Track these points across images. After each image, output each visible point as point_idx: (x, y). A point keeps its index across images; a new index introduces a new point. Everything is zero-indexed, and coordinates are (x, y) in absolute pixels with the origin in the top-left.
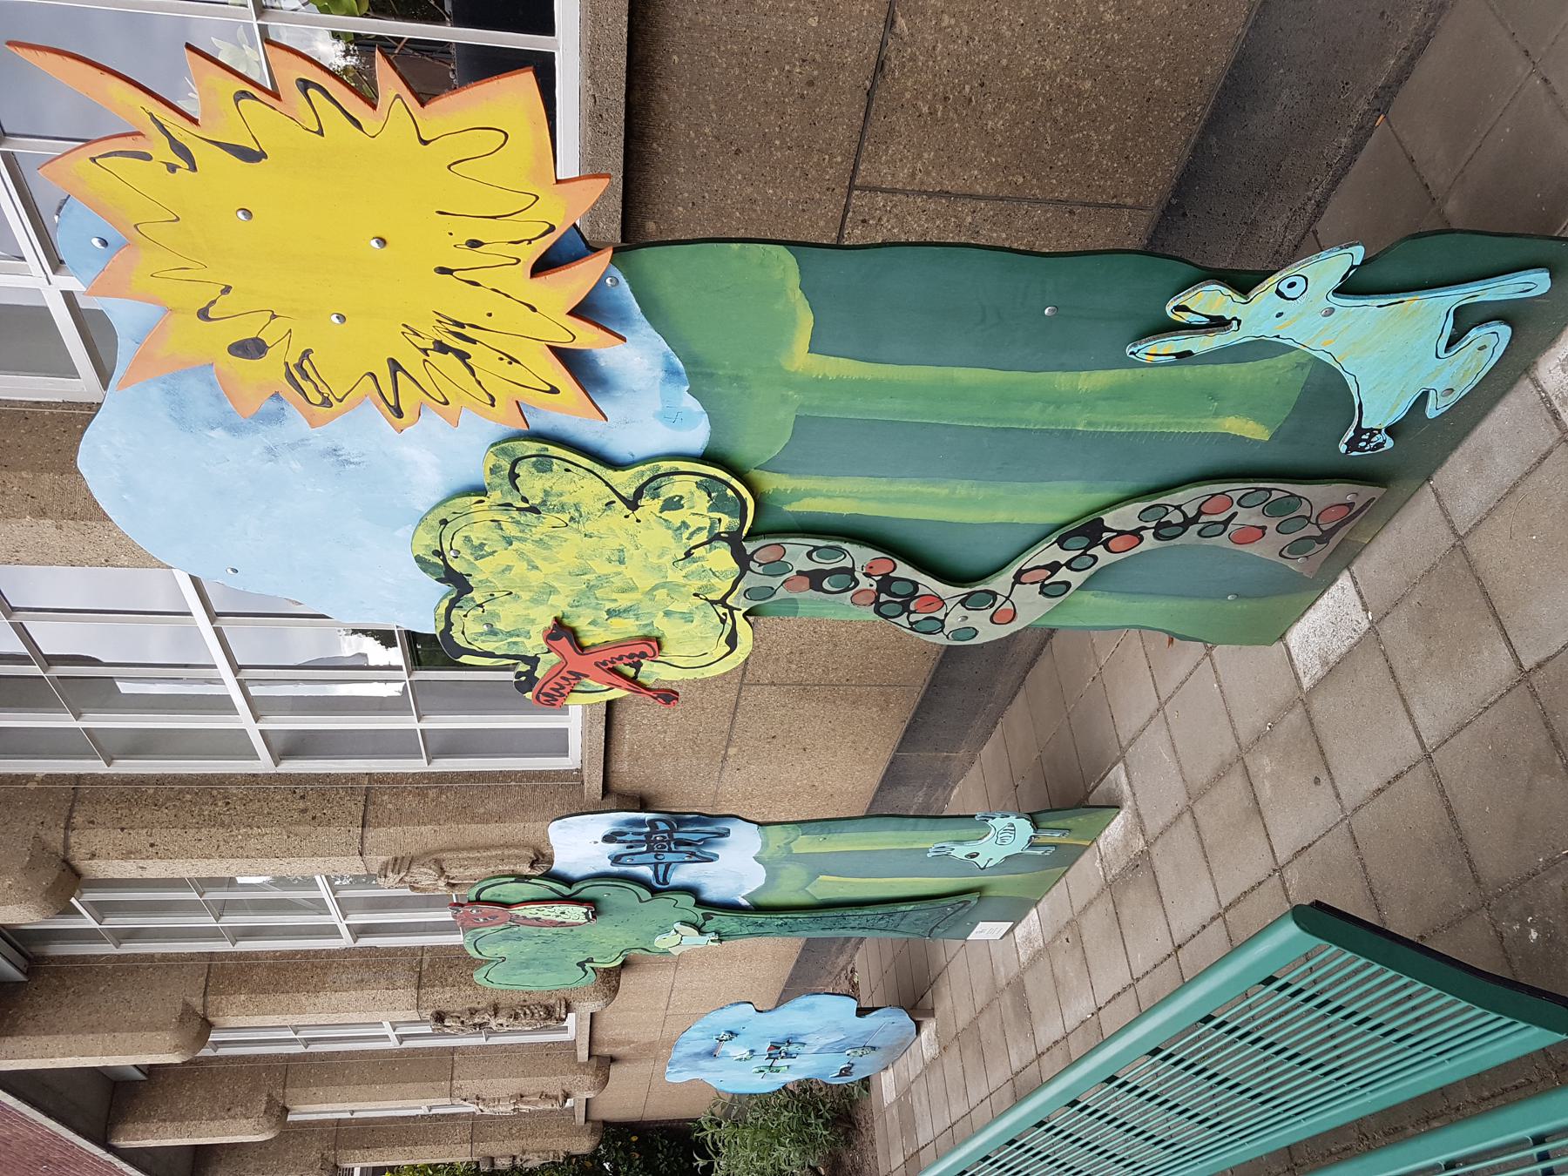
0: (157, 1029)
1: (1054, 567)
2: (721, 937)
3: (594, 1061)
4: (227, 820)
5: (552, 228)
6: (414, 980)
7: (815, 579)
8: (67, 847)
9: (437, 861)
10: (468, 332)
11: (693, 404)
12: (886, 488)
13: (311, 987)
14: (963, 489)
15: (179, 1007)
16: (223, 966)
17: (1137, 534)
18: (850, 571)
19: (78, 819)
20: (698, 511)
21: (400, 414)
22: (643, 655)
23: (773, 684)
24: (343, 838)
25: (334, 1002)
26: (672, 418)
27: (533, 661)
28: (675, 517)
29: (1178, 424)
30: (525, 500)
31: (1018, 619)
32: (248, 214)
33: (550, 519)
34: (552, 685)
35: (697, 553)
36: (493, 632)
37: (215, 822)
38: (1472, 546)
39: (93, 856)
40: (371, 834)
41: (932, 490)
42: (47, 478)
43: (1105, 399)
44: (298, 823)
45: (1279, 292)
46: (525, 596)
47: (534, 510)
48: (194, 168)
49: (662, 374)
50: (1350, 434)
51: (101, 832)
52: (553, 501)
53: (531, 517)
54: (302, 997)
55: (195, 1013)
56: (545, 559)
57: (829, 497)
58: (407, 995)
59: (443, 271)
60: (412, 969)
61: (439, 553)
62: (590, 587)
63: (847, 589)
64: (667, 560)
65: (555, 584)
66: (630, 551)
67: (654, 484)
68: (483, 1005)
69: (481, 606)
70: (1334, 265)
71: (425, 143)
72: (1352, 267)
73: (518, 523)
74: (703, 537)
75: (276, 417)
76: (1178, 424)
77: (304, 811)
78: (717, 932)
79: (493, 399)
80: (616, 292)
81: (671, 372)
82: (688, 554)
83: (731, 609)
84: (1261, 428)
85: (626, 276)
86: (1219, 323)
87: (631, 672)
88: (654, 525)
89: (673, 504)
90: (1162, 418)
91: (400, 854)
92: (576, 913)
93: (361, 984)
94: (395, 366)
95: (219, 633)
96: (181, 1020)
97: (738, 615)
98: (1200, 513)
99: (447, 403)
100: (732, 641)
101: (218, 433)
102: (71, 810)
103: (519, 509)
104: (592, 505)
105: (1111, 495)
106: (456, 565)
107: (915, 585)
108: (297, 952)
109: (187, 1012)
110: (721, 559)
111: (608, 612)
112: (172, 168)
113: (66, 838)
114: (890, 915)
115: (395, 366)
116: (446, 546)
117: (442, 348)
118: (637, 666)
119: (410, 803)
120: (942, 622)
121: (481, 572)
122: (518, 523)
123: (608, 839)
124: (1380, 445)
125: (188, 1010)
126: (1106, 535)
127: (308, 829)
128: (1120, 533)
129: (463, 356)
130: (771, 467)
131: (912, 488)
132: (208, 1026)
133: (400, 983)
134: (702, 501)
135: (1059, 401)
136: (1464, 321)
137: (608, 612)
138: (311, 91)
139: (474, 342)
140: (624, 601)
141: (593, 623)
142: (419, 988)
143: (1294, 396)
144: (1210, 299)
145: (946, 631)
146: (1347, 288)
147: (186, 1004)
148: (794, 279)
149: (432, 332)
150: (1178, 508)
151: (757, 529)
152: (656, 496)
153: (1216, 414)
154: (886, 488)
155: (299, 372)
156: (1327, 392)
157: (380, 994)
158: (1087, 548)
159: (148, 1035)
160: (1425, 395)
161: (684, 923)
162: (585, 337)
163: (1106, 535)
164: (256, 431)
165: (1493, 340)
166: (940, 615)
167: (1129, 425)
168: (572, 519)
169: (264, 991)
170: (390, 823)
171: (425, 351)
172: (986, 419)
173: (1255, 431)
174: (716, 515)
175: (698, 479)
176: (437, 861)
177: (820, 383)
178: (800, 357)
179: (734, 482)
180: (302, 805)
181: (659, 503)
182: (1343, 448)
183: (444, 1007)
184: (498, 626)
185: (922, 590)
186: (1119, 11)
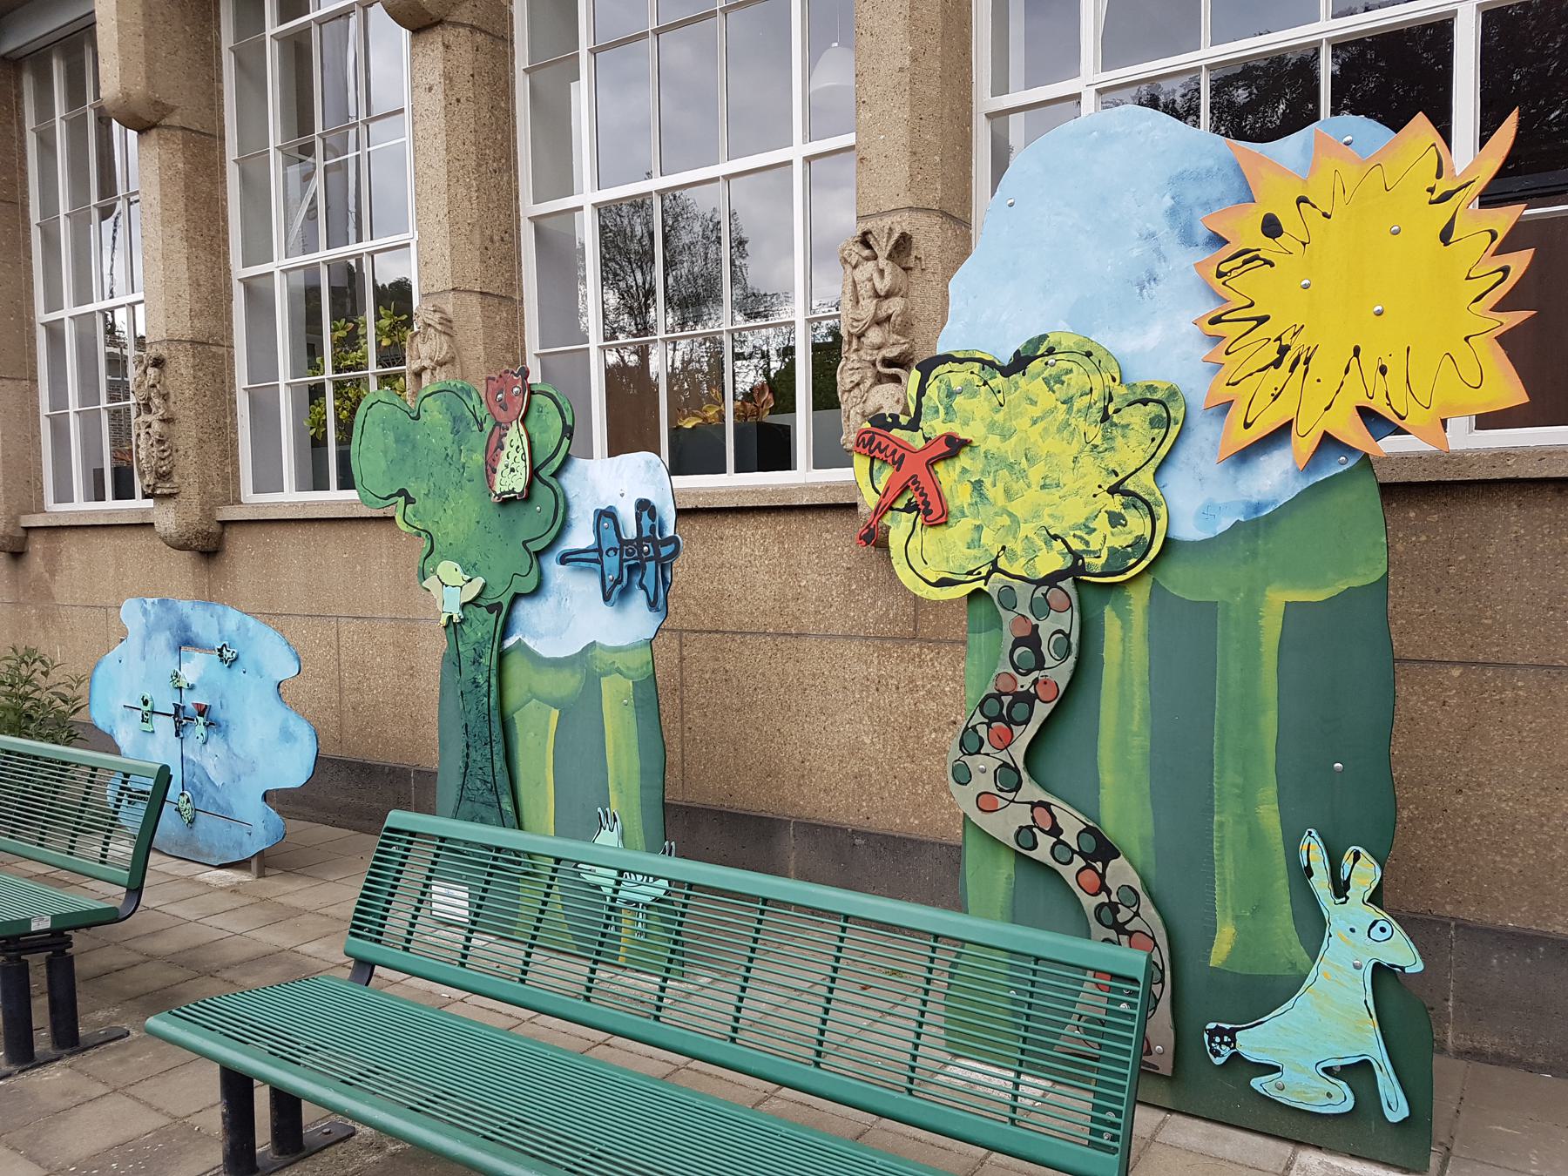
1: (1055, 831)
2: (453, 627)
3: (21, 534)
4: (483, 169)
7: (1031, 640)
8: (455, 24)
10: (1301, 367)
11: (1225, 524)
12: (1137, 681)
14: (1140, 742)
15: (170, 102)
16: (214, 149)
18: (1040, 665)
19: (479, 38)
20: (1104, 541)
21: (1213, 322)
22: (927, 512)
23: (682, 659)
25: (176, 256)
27: (914, 425)
28: (1102, 523)
30: (1117, 411)
32: (1396, 233)
35: (1058, 545)
36: (951, 394)
37: (481, 159)
38: (1155, 1148)
39: (447, 47)
40: (475, 300)
41: (1137, 717)
42: (937, 65)
45: (1375, 922)
46: (999, 417)
47: (1105, 417)
48: (1431, 202)
49: (1254, 500)
50: (1228, 1027)
51: (470, 57)
52: (1117, 432)
53: (1099, 417)
55: (163, 117)
57: (1123, 640)
58: (183, 329)
59: (1357, 351)
60: (211, 336)
61: (1051, 351)
62: (1011, 466)
64: (1047, 521)
65: (1014, 439)
66: (1056, 494)
67: (1139, 503)
68: (173, 408)
69: (985, 383)
70: (1402, 953)
71: (1466, 339)
72: (1402, 969)
73: (1090, 407)
74: (1076, 545)
75: (1187, 238)
77: (492, 240)
78: (463, 621)
81: (1258, 507)
82: (1055, 537)
83: (987, 578)
86: (1340, 888)
87: (901, 504)
89: (1115, 520)
90: (1230, 877)
91: (455, 325)
93: (196, 284)
94: (1262, 320)
95: (716, 179)
97: (980, 584)
99: (1227, 353)
100: (943, 583)
101: (1168, 202)
104: (1112, 461)
105: (1138, 859)
106: (1036, 366)
107: (1027, 722)
108: (225, 220)
110: (1052, 561)
111: (980, 482)
112: (1431, 190)
113: (463, 25)
115: (1262, 320)
117: (1283, 350)
119: (502, 337)
120: (978, 752)
121: (1030, 383)
122: (1090, 407)
123: (644, 506)
124: (1217, 1054)
125: (169, 110)
126: (1099, 865)
127: (478, 242)
128: (1102, 876)
129: (1277, 364)
130: (1156, 588)
131: (1137, 702)
132: (143, 129)
133: (197, 323)
134: (1121, 540)
136: (1358, 1073)
137: (980, 482)
138: (1500, 274)
139: (1292, 370)
142: (192, 342)
143: (1261, 971)
146: (1381, 973)
147: (172, 109)
149: (1297, 346)
150: (1137, 914)
151: (1084, 585)
152: (1125, 506)
153: (1236, 918)
154: (1137, 681)
156: (1267, 992)
157: (185, 304)
158: (1081, 854)
159: (142, 68)
161: (485, 586)
162: (1303, 444)
163: (1099, 865)
164: (1172, 228)
165: (1341, 1099)
166: (986, 748)
168: (1096, 446)
169: (187, 187)
170: (486, 317)
173: (1220, 952)
175: (1148, 536)
178: (1277, 599)
179: (1144, 563)
180: (496, 238)
181: (1118, 509)
182: (1211, 1026)
183: (171, 366)
184: (959, 399)
185: (1017, 730)
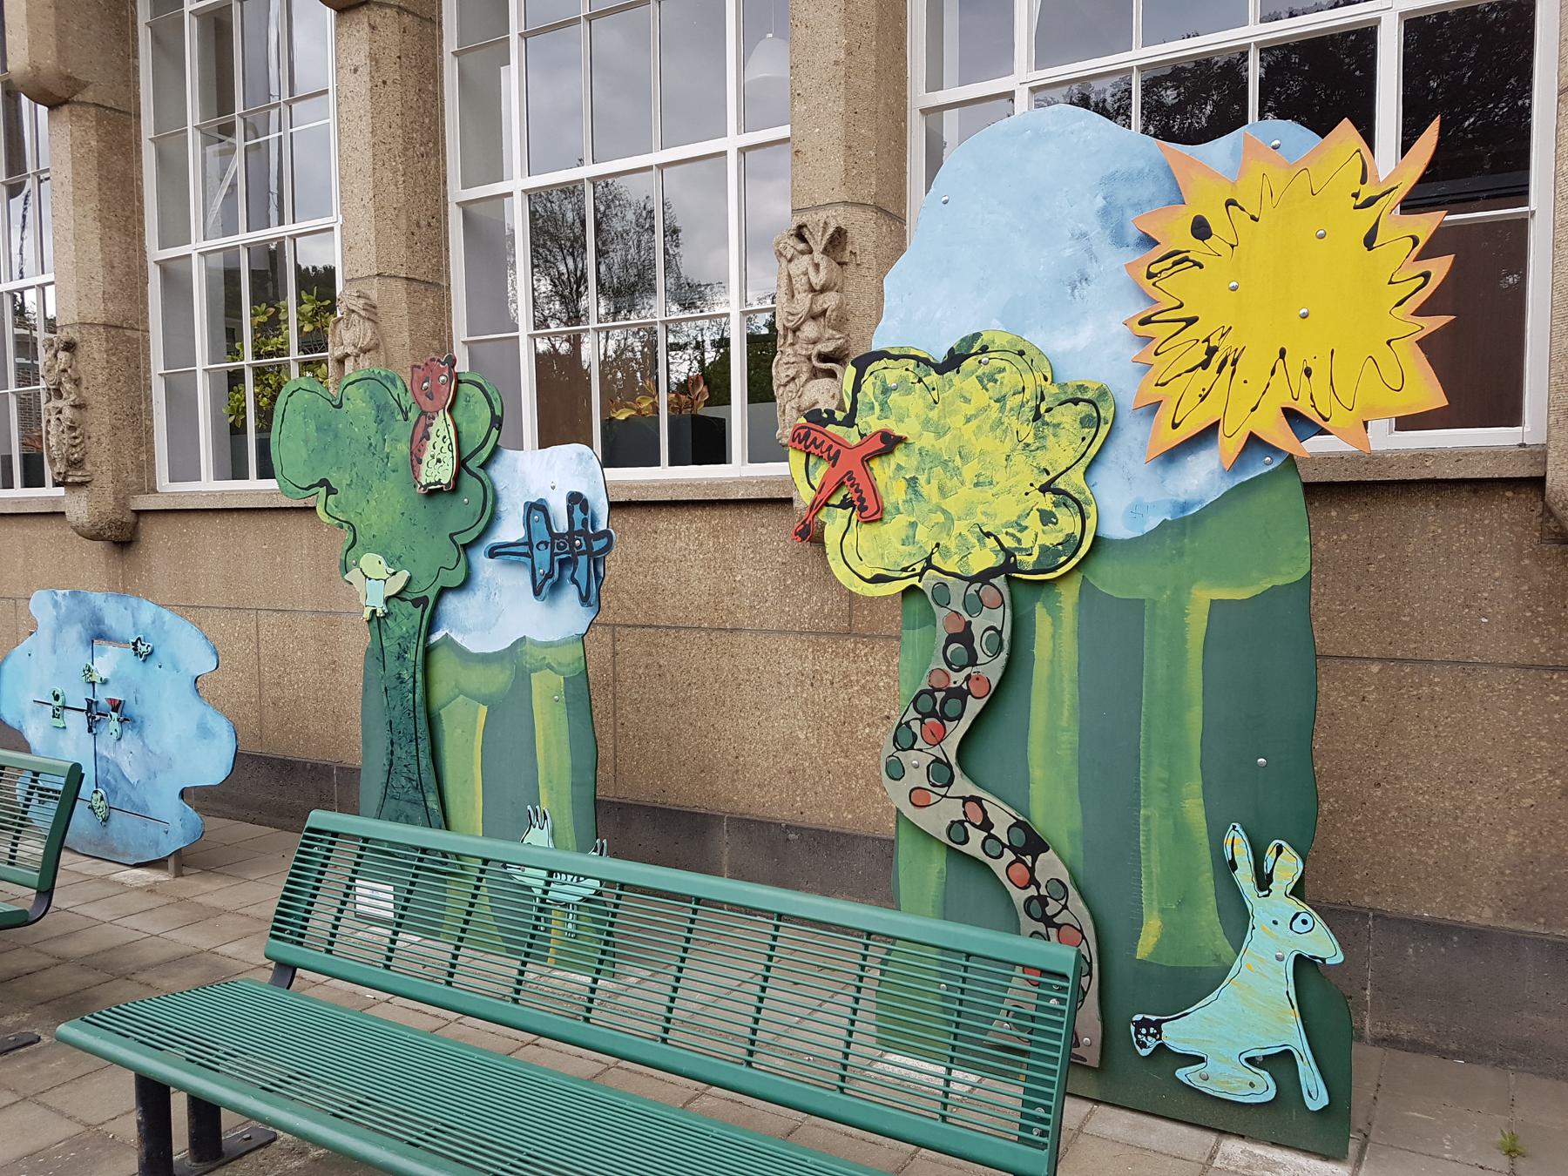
0: (59, 52)
1: (986, 825)
4: (410, 153)
5: (1326, 420)
6: (113, 321)
9: (377, 345)
10: (1228, 368)
11: (1153, 523)
13: (105, 214)
14: (1069, 738)
15: (82, 78)
16: (129, 127)
17: (1033, 881)
18: (973, 661)
19: (407, 19)
20: (1035, 539)
21: (1143, 322)
23: (615, 654)
24: (395, 259)
25: (89, 236)
26: (1136, 511)
27: (849, 421)
29: (1151, 884)
30: (1048, 410)
31: (918, 810)
32: (1321, 237)
33: (1027, 431)
34: (820, 438)
35: (991, 542)
37: (408, 143)
41: (1066, 714)
43: (1175, 824)
44: (408, 218)
46: (934, 414)
47: (1037, 416)
49: (1182, 499)
50: (1154, 1018)
52: (1048, 431)
53: (1031, 415)
54: (94, 204)
55: (76, 92)
56: (979, 427)
57: (1053, 636)
59: (1282, 353)
61: (984, 350)
62: (945, 463)
63: (949, 664)
64: (980, 519)
66: (989, 491)
67: (1070, 502)
68: (85, 393)
69: (920, 380)
70: (1323, 945)
72: (1323, 960)
73: (1022, 406)
74: (1009, 543)
76: (1151, 884)
78: (386, 615)
79: (1163, 384)
80: (1259, 464)
81: (1185, 506)
82: (988, 535)
83: (921, 575)
84: (1150, 949)
85: (1275, 470)
86: (1264, 881)
87: (836, 500)
88: (1022, 507)
89: (1047, 518)
90: (1156, 870)
91: (380, 311)
92: (437, 469)
93: (109, 266)
94: (1191, 321)
95: (649, 168)
96: (69, 78)
98: (1058, 927)
100: (878, 579)
102: (414, 14)
103: (1038, 407)
106: (969, 364)
108: (141, 200)
109: (78, 85)
110: (984, 558)
111: (914, 479)
114: (419, 787)
115: (1191, 321)
116: (992, 355)
117: (1211, 351)
118: (844, 505)
119: (429, 324)
120: (911, 748)
121: (964, 381)
122: (1022, 406)
123: (575, 499)
124: (1143, 1045)
126: (1028, 859)
127: (404, 227)
128: (1032, 870)
129: (1205, 365)
131: (1067, 698)
132: (54, 105)
134: (1051, 538)
135: (1172, 790)
136: (1279, 1063)
137: (914, 479)
138: (1422, 279)
139: (1219, 371)
140: (929, 490)
141: (899, 467)
142: (106, 325)
144: (1287, 867)
145: (898, 754)
147: (85, 85)
148: (1280, 581)
149: (1225, 347)
150: (1065, 907)
151: (1017, 583)
152: (1056, 505)
153: (1162, 911)
155: (1179, 259)
156: (1192, 985)
157: (98, 284)
158: (1011, 847)
160: (1201, 1060)
161: (410, 580)
162: (1230, 444)
163: (1028, 859)
165: (1263, 1088)
167: (1148, 848)
169: (100, 166)
170: (411, 304)
171: (1207, 340)
172: (1148, 740)
173: (1146, 946)
174: (1036, 552)
176: (377, 345)
177: (1181, 612)
178: (1202, 596)
179: (1074, 561)
180: (423, 223)
182: (1138, 1017)
183: (82, 351)
184: (894, 396)
185: (950, 725)
186: (1330, 813)
